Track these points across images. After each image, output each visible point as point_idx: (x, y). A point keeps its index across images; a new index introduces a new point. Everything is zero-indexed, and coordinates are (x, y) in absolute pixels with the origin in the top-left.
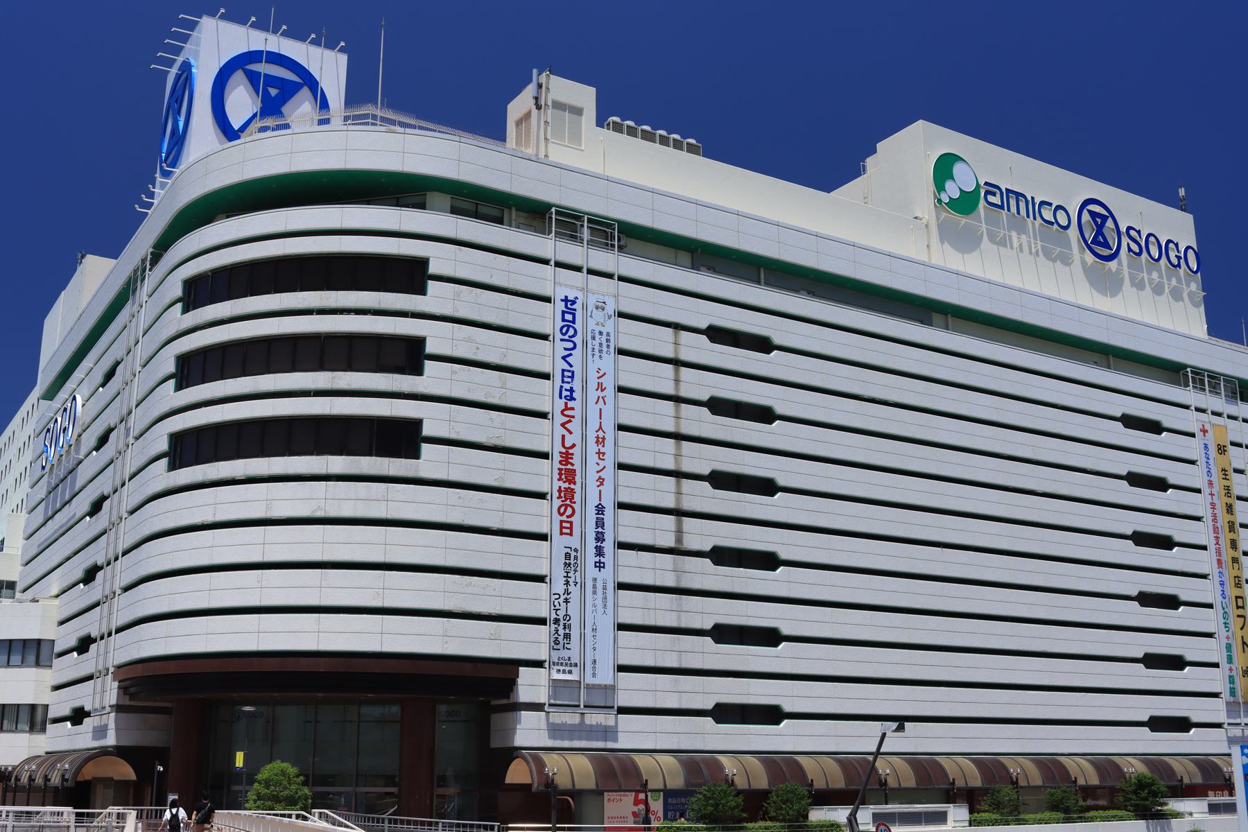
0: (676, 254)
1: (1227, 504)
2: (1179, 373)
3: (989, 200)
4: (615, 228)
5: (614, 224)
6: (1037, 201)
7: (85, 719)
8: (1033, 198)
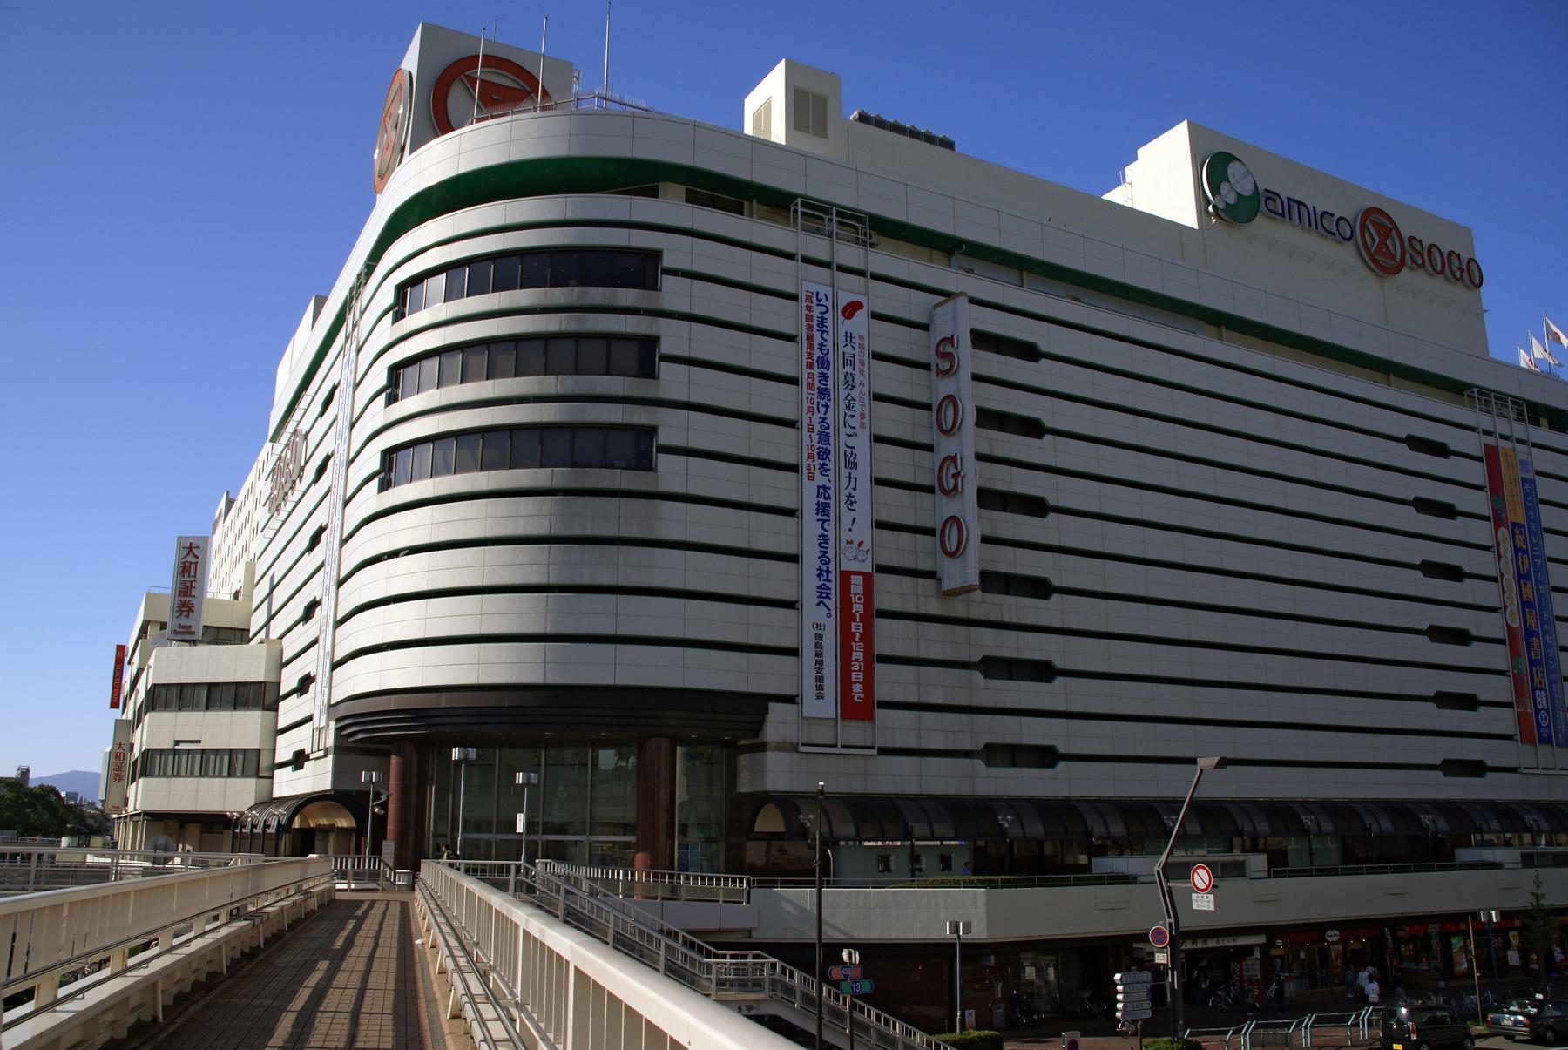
0: (949, 259)
2: (1463, 395)
3: (1271, 208)
4: (866, 222)
5: (866, 218)
6: (1319, 212)
7: (306, 763)
8: (1314, 208)
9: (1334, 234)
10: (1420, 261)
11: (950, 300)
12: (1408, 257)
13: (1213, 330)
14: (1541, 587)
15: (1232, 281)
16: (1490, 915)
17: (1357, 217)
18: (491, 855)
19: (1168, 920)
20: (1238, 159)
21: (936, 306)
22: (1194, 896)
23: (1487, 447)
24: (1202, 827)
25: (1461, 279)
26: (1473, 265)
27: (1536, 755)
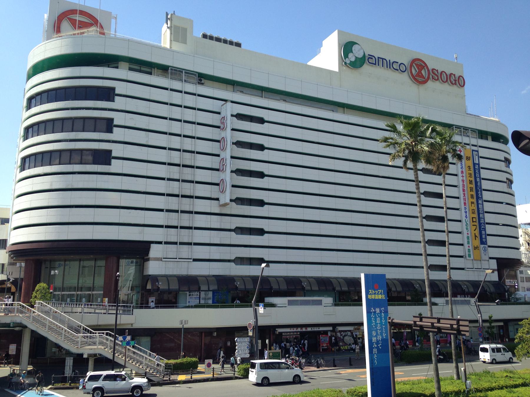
1: (470, 180)
3: (370, 61)
6: (391, 62)
8: (390, 60)
11: (227, 102)
12: (431, 77)
18: (444, 296)
20: (357, 44)
21: (222, 105)
24: (319, 288)
25: (455, 84)
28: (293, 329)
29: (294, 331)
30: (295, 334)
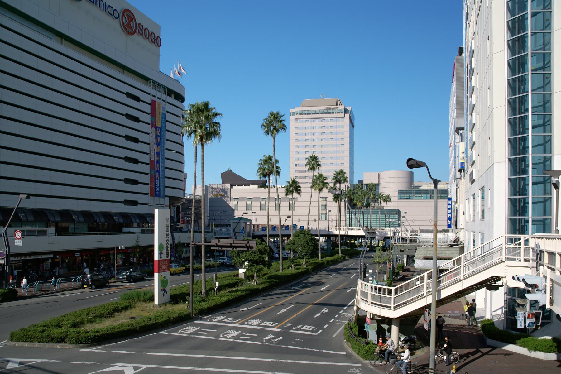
6: (107, 5)
8: (106, 3)
9: (112, 15)
10: (141, 33)
13: (59, 39)
14: (162, 148)
15: (38, 6)
16: (122, 247)
17: (121, 11)
19: (6, 249)
22: (15, 241)
23: (153, 101)
25: (154, 42)
26: (159, 38)
27: (154, 200)
28: (18, 258)
29: (18, 259)
30: (18, 262)
